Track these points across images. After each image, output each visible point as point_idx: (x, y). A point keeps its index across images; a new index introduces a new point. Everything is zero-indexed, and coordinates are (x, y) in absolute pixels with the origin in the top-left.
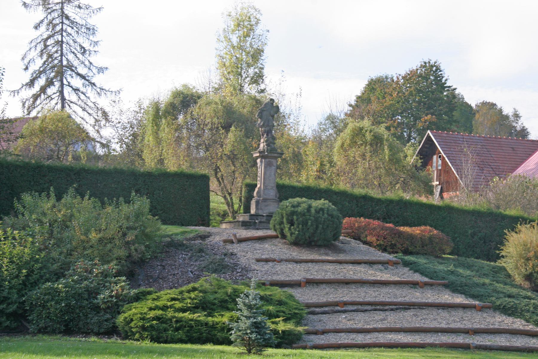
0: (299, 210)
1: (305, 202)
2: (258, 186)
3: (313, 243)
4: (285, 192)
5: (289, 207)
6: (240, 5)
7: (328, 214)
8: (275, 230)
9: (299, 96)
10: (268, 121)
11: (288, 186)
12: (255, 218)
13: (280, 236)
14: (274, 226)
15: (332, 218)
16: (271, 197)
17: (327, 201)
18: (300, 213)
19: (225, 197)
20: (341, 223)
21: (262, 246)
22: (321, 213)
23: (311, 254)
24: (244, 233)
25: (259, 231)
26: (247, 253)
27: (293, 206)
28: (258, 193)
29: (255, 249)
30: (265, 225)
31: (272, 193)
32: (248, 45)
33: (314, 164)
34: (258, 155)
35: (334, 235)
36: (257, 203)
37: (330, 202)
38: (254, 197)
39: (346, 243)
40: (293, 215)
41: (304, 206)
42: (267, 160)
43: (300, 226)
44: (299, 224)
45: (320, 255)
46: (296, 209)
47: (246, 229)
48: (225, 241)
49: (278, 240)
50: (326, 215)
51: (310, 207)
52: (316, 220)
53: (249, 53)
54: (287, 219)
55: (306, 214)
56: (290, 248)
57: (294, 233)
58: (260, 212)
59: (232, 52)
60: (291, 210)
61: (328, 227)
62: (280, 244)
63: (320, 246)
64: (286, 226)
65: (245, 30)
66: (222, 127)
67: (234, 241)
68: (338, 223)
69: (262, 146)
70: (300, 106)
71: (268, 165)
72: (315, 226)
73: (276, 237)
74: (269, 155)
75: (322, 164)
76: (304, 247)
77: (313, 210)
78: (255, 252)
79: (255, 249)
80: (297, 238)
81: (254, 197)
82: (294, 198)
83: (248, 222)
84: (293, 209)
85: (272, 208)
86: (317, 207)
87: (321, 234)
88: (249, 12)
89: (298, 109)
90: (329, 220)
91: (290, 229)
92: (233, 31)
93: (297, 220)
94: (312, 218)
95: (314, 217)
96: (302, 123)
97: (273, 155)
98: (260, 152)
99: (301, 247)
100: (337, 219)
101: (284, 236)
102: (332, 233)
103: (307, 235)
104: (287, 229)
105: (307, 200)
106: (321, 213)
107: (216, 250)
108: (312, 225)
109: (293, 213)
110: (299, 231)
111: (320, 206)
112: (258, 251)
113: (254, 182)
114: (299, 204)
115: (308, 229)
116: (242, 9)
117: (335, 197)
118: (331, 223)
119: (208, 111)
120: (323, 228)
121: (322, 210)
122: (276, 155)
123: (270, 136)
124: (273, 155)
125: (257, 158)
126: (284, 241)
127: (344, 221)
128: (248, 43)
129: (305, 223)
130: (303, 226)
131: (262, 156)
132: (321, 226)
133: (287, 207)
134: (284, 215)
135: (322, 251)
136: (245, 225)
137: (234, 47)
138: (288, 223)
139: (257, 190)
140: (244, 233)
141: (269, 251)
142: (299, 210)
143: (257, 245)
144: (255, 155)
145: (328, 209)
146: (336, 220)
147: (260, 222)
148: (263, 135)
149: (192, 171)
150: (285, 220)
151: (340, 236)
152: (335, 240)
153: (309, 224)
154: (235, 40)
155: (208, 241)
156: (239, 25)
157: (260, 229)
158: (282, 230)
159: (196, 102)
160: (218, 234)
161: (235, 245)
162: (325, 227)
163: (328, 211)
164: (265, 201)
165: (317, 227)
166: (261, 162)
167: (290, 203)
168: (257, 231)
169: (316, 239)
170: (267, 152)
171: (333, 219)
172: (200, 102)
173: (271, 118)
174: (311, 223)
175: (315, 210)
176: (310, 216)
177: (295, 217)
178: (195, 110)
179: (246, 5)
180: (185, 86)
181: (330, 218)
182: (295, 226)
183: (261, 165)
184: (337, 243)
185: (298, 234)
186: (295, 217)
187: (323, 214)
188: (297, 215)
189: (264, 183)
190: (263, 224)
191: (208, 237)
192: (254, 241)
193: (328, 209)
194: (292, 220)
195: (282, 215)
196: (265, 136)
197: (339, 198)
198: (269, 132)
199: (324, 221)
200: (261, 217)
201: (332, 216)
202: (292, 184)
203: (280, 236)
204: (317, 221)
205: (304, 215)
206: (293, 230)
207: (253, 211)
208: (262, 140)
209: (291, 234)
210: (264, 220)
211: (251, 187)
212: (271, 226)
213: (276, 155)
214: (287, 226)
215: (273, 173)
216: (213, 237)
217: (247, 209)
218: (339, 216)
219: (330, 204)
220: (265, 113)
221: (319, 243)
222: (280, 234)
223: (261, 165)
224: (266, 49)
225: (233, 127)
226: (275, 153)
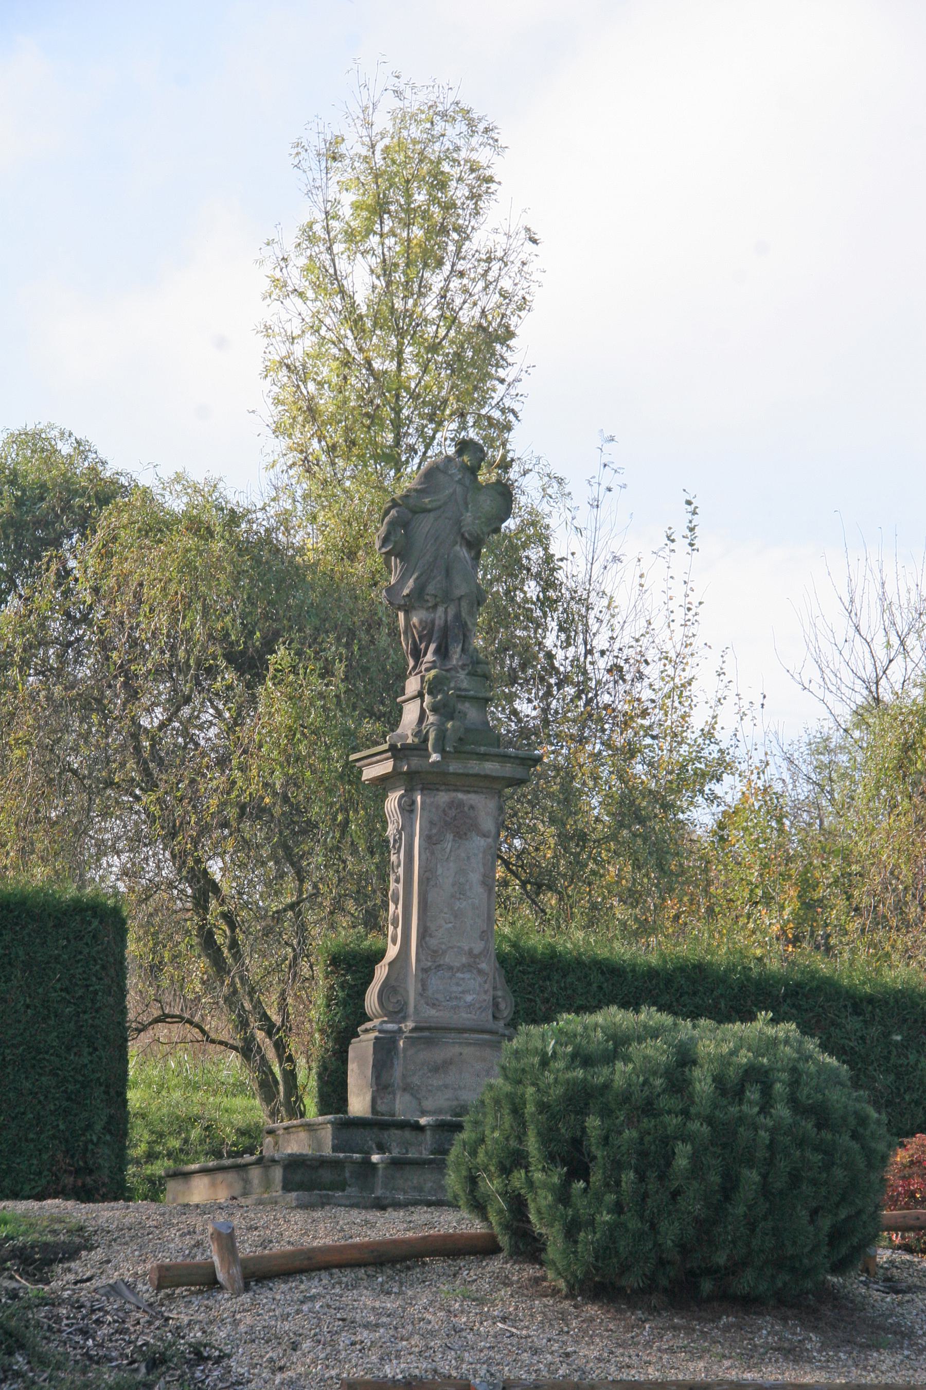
0: (619, 1081)
1: (654, 1033)
2: (392, 951)
3: (707, 1286)
4: (539, 984)
5: (560, 1064)
6: (390, 102)
7: (793, 1101)
8: (479, 1207)
9: (681, 545)
10: (448, 573)
11: (579, 962)
12: (368, 1137)
13: (504, 1240)
14: (472, 1181)
15: (819, 1126)
16: (465, 1017)
17: (788, 1029)
18: (626, 1098)
19: (248, 1050)
20: (881, 1161)
21: (390, 1304)
22: (753, 1094)
23: (695, 1355)
24: (299, 1228)
25: (390, 1214)
26: (295, 1347)
27: (583, 1059)
28: (387, 989)
29: (349, 1324)
30: (427, 1179)
31: (474, 994)
32: (432, 313)
33: (768, 899)
34: (386, 767)
35: (837, 1235)
36: (385, 1048)
37: (806, 1029)
38: (365, 1018)
39: (909, 1290)
40: (583, 1112)
41: (655, 1051)
42: (443, 798)
43: (628, 1177)
44: (618, 1166)
45: (750, 1358)
46: (601, 1075)
47: (302, 1206)
48: (168, 1279)
49: (495, 1265)
50: (782, 1111)
51: (685, 1058)
52: (724, 1135)
53: (434, 348)
54: (547, 1137)
55: (665, 1102)
56: (563, 1317)
57: (591, 1223)
58: (401, 1107)
59: (350, 344)
60: (574, 1082)
61: (795, 1179)
62: (505, 1292)
63: (748, 1304)
64: (538, 1176)
65: (417, 232)
66: (230, 657)
67: (221, 1276)
68: (861, 1164)
69: (410, 713)
70: (694, 599)
71: (452, 826)
72: (715, 1179)
73: (485, 1248)
74: (454, 767)
75: (810, 907)
76: (654, 1311)
77: (702, 1083)
78: (344, 1339)
79: (349, 1324)
80: (604, 1252)
81: (365, 1018)
82: (592, 1009)
83: (323, 1162)
84: (580, 1073)
85: (475, 1080)
86: (725, 1061)
87: (752, 1227)
88: (433, 139)
89: (679, 616)
90: (801, 1143)
91: (563, 1196)
92: (350, 236)
93: (606, 1141)
94: (695, 1126)
95: (710, 1120)
96: (704, 688)
97: (474, 767)
98: (396, 752)
99: (633, 1307)
100: (855, 1136)
101: (528, 1247)
102: (826, 1223)
103: (670, 1232)
104: (545, 1199)
105: (666, 1019)
106: (753, 1094)
107: (105, 1330)
108: (697, 1169)
109: (581, 1099)
110: (618, 1208)
111: (744, 1057)
112: (364, 1335)
113: (370, 941)
114: (618, 1045)
115: (675, 1194)
116: (403, 119)
117: (853, 1023)
118: (816, 1158)
119: (152, 569)
120: (765, 1189)
121: (755, 1075)
122: (491, 767)
123: (456, 658)
124: (474, 767)
125: (384, 783)
126: (531, 1271)
127: (901, 1156)
128: (432, 299)
129: (653, 1159)
130: (642, 1178)
131: (413, 777)
132: (752, 1176)
133: (545, 1063)
134: (530, 1108)
135: (766, 1330)
136: (308, 1179)
137: (356, 322)
138: (551, 1157)
139: (381, 972)
140: (299, 1228)
141: (432, 1334)
142: (619, 1081)
143: (365, 1301)
144: (370, 773)
145: (794, 1070)
146: (845, 1140)
147: (397, 1164)
148: (417, 655)
149: (797, 1382)
150: (532, 1144)
151: (871, 1240)
152: (839, 1267)
153: (682, 1162)
154: (361, 279)
155: (62, 1281)
156: (380, 208)
157: (397, 1205)
158: (518, 1205)
159: (85, 524)
160: (133, 1233)
161: (225, 1303)
162: (779, 1183)
163: (795, 1083)
164: (430, 1042)
165: (730, 1187)
166: (407, 809)
167: (564, 1037)
168: (373, 1215)
169: (721, 1259)
170: (440, 747)
171: (827, 1135)
172: (107, 519)
173: (463, 553)
174: (695, 1158)
175: (718, 1080)
176: (685, 1113)
177: (593, 1122)
178: (79, 557)
179: (414, 102)
180: (33, 441)
181: (808, 1125)
182: (596, 1178)
183: (407, 827)
184: (853, 1283)
185: (613, 1227)
186: (593, 1122)
187: (765, 1107)
188: (606, 1113)
189: (424, 933)
190: (415, 1178)
191: (71, 1253)
192: (348, 1276)
193: (794, 1070)
194: (577, 1143)
195: (517, 1112)
196: (429, 657)
197: (874, 1031)
198: (448, 637)
199: (771, 1146)
200: (408, 1134)
201: (821, 1115)
202: (603, 953)
203: (504, 1240)
204: (724, 1135)
205: (649, 1108)
206: (581, 1203)
207: (359, 1104)
208: (412, 685)
209: (572, 1230)
210: (423, 1150)
211: (355, 966)
212: (453, 1181)
213: (491, 767)
214: (542, 1178)
215: (475, 877)
216: (97, 1255)
217: (333, 1093)
218: (863, 1120)
219: (811, 1045)
220: (425, 525)
221: (746, 1282)
222: (506, 1227)
223: (407, 827)
224: (525, 327)
225: (282, 651)
226: (484, 757)
